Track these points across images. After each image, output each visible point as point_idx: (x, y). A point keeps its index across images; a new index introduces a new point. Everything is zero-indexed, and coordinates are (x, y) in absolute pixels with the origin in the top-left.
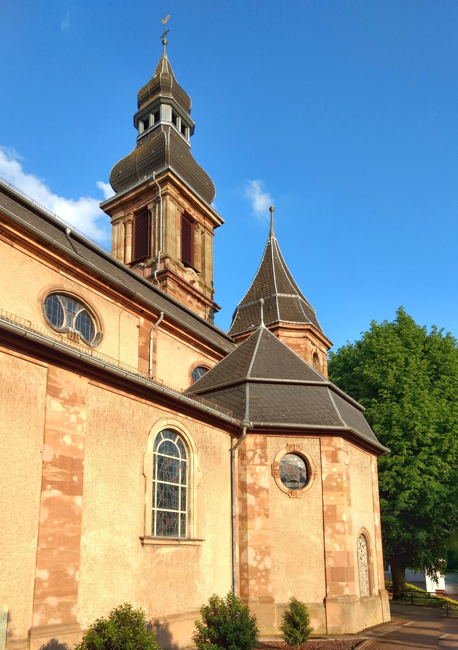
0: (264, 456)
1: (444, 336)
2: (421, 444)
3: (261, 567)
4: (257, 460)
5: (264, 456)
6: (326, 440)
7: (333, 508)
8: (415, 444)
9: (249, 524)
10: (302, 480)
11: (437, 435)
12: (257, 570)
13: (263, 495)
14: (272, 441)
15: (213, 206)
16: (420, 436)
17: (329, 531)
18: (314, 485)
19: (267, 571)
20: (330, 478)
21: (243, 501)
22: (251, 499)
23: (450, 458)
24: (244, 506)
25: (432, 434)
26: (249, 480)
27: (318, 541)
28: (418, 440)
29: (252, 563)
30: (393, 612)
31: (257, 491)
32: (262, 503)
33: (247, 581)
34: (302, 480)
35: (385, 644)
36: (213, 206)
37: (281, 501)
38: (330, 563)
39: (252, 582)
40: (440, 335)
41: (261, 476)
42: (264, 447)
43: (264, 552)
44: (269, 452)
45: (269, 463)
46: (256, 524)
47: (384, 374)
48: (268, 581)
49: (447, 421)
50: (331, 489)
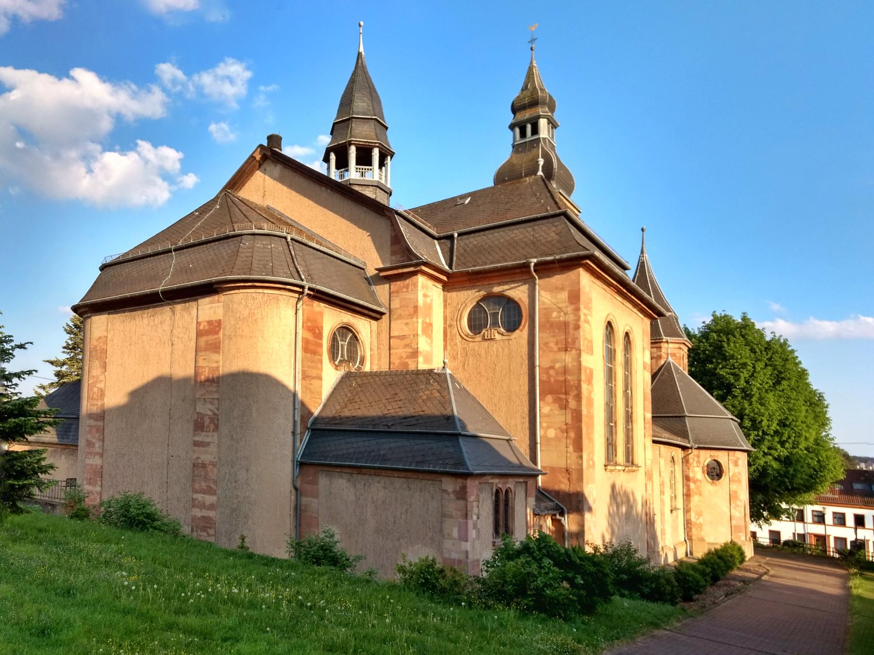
0: (698, 462)
1: (782, 341)
2: (764, 433)
3: (698, 522)
4: (695, 464)
5: (698, 462)
6: (731, 453)
7: (735, 492)
8: (760, 433)
9: (692, 499)
10: (717, 475)
11: (778, 428)
12: (696, 523)
13: (698, 483)
14: (702, 452)
15: (572, 198)
16: (765, 428)
17: (733, 505)
18: (725, 479)
19: (701, 524)
20: (734, 475)
21: (688, 486)
22: (692, 485)
23: (787, 445)
24: (689, 489)
25: (774, 426)
26: (691, 475)
27: (727, 510)
28: (763, 431)
29: (693, 519)
30: (755, 553)
31: (695, 481)
32: (698, 488)
33: (691, 529)
34: (717, 475)
35: (292, 510)
36: (572, 198)
37: (707, 486)
38: (734, 522)
39: (693, 530)
40: (779, 339)
41: (698, 473)
42: (698, 457)
43: (699, 514)
44: (702, 460)
45: (701, 465)
46: (695, 500)
47: (737, 376)
48: (701, 529)
49: (787, 419)
50: (734, 481)
